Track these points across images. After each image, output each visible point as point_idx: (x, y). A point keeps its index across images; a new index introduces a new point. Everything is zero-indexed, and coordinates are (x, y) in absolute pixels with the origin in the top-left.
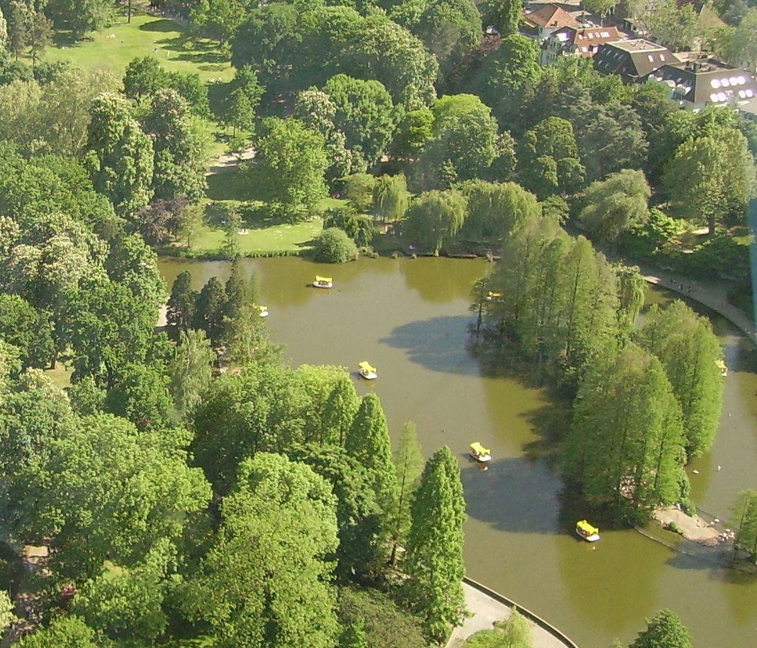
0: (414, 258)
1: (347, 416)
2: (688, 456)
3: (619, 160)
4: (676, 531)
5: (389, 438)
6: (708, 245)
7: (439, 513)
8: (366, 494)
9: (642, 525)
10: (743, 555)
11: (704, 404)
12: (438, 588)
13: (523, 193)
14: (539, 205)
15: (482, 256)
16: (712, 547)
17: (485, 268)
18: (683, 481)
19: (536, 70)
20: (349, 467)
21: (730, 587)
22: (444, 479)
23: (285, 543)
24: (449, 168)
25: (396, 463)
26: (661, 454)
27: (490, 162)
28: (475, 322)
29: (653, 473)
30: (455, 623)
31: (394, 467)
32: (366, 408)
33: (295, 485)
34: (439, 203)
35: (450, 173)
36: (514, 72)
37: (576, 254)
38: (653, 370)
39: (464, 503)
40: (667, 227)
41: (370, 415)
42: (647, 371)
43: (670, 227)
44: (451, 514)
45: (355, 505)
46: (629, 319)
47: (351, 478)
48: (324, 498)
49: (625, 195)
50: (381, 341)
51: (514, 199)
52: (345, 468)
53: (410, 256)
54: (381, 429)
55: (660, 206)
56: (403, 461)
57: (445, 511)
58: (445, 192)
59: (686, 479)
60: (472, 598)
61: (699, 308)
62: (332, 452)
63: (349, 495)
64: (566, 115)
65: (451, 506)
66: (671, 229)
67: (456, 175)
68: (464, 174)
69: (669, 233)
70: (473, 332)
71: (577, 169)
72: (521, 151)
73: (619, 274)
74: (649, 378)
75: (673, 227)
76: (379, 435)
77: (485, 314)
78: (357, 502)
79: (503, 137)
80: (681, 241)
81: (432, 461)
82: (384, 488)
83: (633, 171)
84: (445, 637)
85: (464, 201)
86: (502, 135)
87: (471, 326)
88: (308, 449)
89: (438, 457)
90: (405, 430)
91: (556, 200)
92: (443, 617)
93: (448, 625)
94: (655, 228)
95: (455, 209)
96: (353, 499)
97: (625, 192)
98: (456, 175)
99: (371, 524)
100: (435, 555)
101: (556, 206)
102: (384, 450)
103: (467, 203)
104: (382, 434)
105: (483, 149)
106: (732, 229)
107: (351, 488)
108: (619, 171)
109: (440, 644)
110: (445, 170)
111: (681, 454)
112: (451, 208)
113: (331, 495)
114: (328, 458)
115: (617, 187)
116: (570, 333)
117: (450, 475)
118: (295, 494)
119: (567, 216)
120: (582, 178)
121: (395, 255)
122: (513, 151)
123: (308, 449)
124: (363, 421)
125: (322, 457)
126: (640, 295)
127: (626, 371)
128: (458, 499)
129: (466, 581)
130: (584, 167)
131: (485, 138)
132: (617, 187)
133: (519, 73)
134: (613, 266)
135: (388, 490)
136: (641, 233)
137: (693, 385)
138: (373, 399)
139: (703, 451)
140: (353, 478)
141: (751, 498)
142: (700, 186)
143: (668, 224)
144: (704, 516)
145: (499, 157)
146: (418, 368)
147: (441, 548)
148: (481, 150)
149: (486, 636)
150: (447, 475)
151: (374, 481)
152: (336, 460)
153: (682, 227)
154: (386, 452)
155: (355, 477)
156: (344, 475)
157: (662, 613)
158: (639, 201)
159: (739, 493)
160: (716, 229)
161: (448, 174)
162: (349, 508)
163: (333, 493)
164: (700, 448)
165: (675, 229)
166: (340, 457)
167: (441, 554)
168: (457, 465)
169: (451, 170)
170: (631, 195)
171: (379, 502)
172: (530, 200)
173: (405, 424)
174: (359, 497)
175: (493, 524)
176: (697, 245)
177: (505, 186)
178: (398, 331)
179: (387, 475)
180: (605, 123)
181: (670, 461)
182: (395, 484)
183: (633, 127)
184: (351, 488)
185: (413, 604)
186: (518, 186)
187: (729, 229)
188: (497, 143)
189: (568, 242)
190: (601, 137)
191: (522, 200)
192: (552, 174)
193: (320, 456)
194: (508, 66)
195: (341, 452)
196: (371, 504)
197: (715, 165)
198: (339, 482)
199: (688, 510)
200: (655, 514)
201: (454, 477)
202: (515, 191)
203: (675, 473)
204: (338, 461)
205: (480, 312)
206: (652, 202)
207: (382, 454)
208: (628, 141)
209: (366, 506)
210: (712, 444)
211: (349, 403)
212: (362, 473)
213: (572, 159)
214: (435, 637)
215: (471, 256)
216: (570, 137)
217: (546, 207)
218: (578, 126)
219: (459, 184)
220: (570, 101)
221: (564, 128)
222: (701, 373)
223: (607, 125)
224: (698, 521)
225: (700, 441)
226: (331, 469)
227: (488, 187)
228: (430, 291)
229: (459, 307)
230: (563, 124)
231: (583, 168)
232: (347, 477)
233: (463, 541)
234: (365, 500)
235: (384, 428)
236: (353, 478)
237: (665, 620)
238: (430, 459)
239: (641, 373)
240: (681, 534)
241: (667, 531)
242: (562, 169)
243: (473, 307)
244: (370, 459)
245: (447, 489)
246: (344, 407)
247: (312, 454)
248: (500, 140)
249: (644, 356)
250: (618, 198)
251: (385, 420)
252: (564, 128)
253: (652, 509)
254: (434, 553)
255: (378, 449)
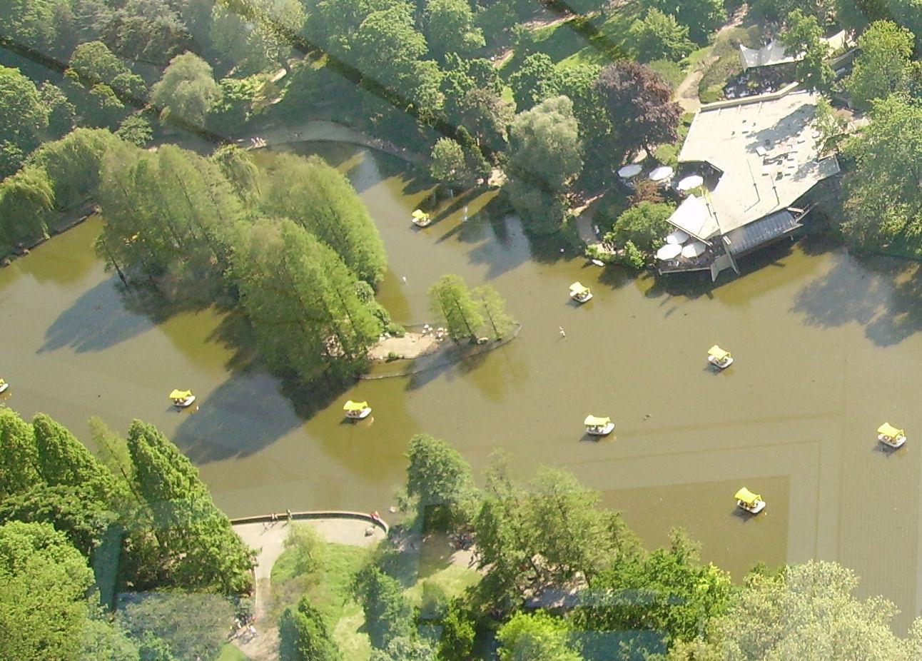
0: (27, 253)
1: (30, 449)
2: (372, 286)
3: (167, 51)
4: (398, 358)
5: (82, 445)
6: (289, 86)
7: (166, 483)
8: (92, 509)
9: (367, 372)
10: (465, 342)
11: (355, 235)
12: (212, 549)
13: (93, 133)
14: (116, 135)
15: (92, 213)
16: (435, 352)
17: (91, 231)
18: (378, 311)
19: (43, 7)
20: (59, 497)
21: (472, 373)
22: (149, 450)
23: (33, 609)
24: (10, 148)
25: (105, 462)
26: (342, 300)
27: (46, 121)
28: (118, 280)
29: (347, 321)
30: (250, 567)
31: (104, 467)
32: (41, 432)
33: (13, 548)
34: (17, 188)
35: (13, 152)
36: (23, 20)
37: (165, 162)
38: (288, 233)
39: (186, 459)
40: (244, 90)
41: (49, 435)
42: (284, 236)
43: (246, 88)
44: (178, 478)
45: (87, 527)
46: (255, 194)
47: (67, 504)
48: (52, 540)
49: (187, 82)
50: (40, 351)
51: (89, 145)
52: (55, 499)
53: (23, 254)
54: (69, 442)
55: (232, 73)
56: (110, 456)
57: (170, 478)
58: (18, 175)
59: (379, 307)
60: (250, 535)
61: (305, 149)
62: (37, 494)
63: (75, 521)
64: (91, 36)
65: (174, 470)
66: (249, 89)
67: (20, 151)
68: (29, 145)
69: (249, 94)
70: (122, 290)
71: (132, 81)
72: (73, 95)
73: (220, 159)
74: (290, 241)
75: (249, 87)
76: (69, 448)
77: (122, 267)
78: (88, 522)
79: (45, 90)
80: (264, 95)
81: (131, 441)
82: (108, 492)
83: (181, 56)
84: (250, 585)
85: (42, 172)
86: (43, 89)
87: (117, 285)
88: (9, 505)
89: (135, 434)
90: (93, 428)
91: (131, 121)
92: (236, 570)
93: (246, 573)
94: (235, 97)
95: (38, 184)
96: (83, 523)
97: (186, 78)
98: (20, 151)
99: (117, 533)
100: (190, 522)
101: (134, 127)
102: (84, 458)
103: (45, 172)
104: (73, 445)
105: (31, 111)
106: (306, 58)
107: (73, 515)
108: (169, 64)
109: (249, 594)
110: (7, 152)
111: (364, 287)
112: (33, 185)
113: (57, 533)
114: (33, 500)
115: (177, 78)
116: (207, 239)
117: (156, 443)
118: (19, 557)
119: (150, 130)
120: (143, 86)
121: (7, 261)
122: (63, 97)
123: (9, 505)
124: (47, 444)
125: (27, 503)
126: (251, 167)
127: (266, 247)
128: (178, 459)
129: (234, 523)
130: (138, 76)
131: (26, 101)
132: (177, 78)
133: (28, 18)
134: (211, 155)
135: (113, 492)
136: (225, 108)
137: (337, 221)
138: (43, 419)
139: (382, 273)
140: (69, 503)
141: (439, 290)
142: (252, 35)
143: (244, 86)
144: (413, 330)
145: (52, 111)
146: (90, 356)
147: (190, 513)
148: (30, 114)
149: (286, 559)
150: (152, 444)
151: (93, 492)
152: (42, 498)
153: (257, 82)
154: (87, 458)
155: (68, 503)
156: (59, 507)
157: (414, 442)
158: (204, 81)
159: (428, 293)
160: (291, 66)
161: (12, 155)
162: (85, 533)
163: (57, 531)
164: (377, 272)
165: (252, 87)
166: (45, 492)
167: (194, 518)
168: (156, 430)
169: (12, 150)
170: (193, 79)
171: (114, 507)
172: (104, 135)
173: (89, 421)
174: (88, 517)
175: (237, 455)
176: (281, 90)
177: (69, 138)
178: (50, 332)
179: (103, 479)
180: (132, 24)
181: (354, 302)
182: (116, 482)
183: (161, 13)
184: (73, 515)
185: (200, 578)
186: (84, 129)
187: (303, 59)
188: (42, 99)
189: (152, 155)
190: (137, 39)
191: (96, 140)
192: (112, 99)
193: (25, 504)
194: (13, 18)
195: (42, 487)
196: (103, 516)
197: (254, 10)
198: (59, 516)
199: (398, 333)
200: (371, 355)
201: (160, 442)
202: (82, 135)
203: (367, 310)
204: (45, 498)
205: (117, 267)
206: (218, 75)
207: (85, 463)
208: (166, 29)
209: (99, 520)
210: (386, 262)
211: (25, 436)
212: (77, 493)
213: (123, 75)
214: (241, 591)
215: (81, 219)
216: (108, 54)
217: (125, 133)
218: (111, 41)
219: (29, 158)
220: (89, 21)
221: (97, 50)
222: (338, 207)
223: (135, 25)
224: (411, 337)
225: (373, 266)
226: (42, 509)
227: (56, 146)
228: (66, 272)
229: (98, 275)
230: (94, 46)
231: (138, 78)
232: (63, 507)
233: (209, 492)
234: (95, 516)
235: (71, 438)
236: (69, 503)
237: (419, 445)
238: (128, 440)
239: (281, 242)
240: (403, 358)
241: (390, 363)
242: (118, 92)
243: (107, 268)
244: (76, 476)
245: (159, 458)
246: (22, 442)
247: (16, 507)
248: (43, 95)
249: (275, 223)
250: (184, 88)
251: (67, 431)
252: (97, 50)
253: (366, 352)
254: (187, 521)
255: (78, 461)
